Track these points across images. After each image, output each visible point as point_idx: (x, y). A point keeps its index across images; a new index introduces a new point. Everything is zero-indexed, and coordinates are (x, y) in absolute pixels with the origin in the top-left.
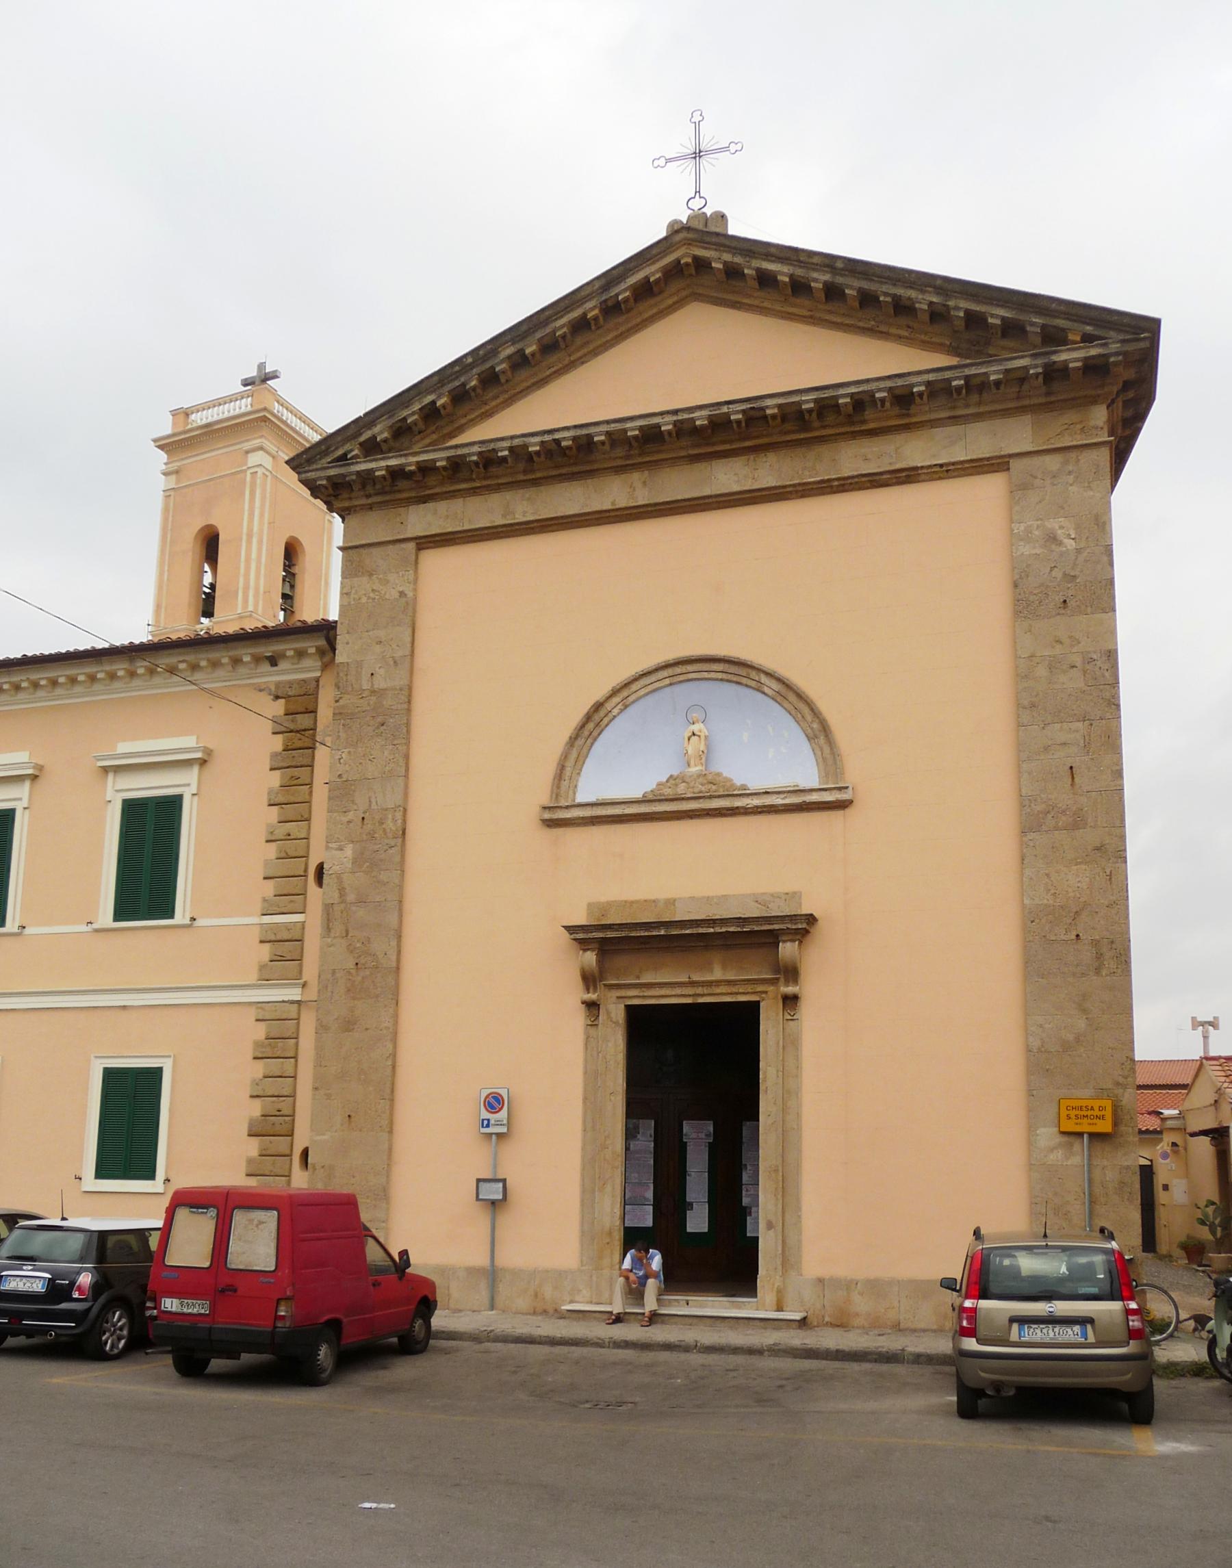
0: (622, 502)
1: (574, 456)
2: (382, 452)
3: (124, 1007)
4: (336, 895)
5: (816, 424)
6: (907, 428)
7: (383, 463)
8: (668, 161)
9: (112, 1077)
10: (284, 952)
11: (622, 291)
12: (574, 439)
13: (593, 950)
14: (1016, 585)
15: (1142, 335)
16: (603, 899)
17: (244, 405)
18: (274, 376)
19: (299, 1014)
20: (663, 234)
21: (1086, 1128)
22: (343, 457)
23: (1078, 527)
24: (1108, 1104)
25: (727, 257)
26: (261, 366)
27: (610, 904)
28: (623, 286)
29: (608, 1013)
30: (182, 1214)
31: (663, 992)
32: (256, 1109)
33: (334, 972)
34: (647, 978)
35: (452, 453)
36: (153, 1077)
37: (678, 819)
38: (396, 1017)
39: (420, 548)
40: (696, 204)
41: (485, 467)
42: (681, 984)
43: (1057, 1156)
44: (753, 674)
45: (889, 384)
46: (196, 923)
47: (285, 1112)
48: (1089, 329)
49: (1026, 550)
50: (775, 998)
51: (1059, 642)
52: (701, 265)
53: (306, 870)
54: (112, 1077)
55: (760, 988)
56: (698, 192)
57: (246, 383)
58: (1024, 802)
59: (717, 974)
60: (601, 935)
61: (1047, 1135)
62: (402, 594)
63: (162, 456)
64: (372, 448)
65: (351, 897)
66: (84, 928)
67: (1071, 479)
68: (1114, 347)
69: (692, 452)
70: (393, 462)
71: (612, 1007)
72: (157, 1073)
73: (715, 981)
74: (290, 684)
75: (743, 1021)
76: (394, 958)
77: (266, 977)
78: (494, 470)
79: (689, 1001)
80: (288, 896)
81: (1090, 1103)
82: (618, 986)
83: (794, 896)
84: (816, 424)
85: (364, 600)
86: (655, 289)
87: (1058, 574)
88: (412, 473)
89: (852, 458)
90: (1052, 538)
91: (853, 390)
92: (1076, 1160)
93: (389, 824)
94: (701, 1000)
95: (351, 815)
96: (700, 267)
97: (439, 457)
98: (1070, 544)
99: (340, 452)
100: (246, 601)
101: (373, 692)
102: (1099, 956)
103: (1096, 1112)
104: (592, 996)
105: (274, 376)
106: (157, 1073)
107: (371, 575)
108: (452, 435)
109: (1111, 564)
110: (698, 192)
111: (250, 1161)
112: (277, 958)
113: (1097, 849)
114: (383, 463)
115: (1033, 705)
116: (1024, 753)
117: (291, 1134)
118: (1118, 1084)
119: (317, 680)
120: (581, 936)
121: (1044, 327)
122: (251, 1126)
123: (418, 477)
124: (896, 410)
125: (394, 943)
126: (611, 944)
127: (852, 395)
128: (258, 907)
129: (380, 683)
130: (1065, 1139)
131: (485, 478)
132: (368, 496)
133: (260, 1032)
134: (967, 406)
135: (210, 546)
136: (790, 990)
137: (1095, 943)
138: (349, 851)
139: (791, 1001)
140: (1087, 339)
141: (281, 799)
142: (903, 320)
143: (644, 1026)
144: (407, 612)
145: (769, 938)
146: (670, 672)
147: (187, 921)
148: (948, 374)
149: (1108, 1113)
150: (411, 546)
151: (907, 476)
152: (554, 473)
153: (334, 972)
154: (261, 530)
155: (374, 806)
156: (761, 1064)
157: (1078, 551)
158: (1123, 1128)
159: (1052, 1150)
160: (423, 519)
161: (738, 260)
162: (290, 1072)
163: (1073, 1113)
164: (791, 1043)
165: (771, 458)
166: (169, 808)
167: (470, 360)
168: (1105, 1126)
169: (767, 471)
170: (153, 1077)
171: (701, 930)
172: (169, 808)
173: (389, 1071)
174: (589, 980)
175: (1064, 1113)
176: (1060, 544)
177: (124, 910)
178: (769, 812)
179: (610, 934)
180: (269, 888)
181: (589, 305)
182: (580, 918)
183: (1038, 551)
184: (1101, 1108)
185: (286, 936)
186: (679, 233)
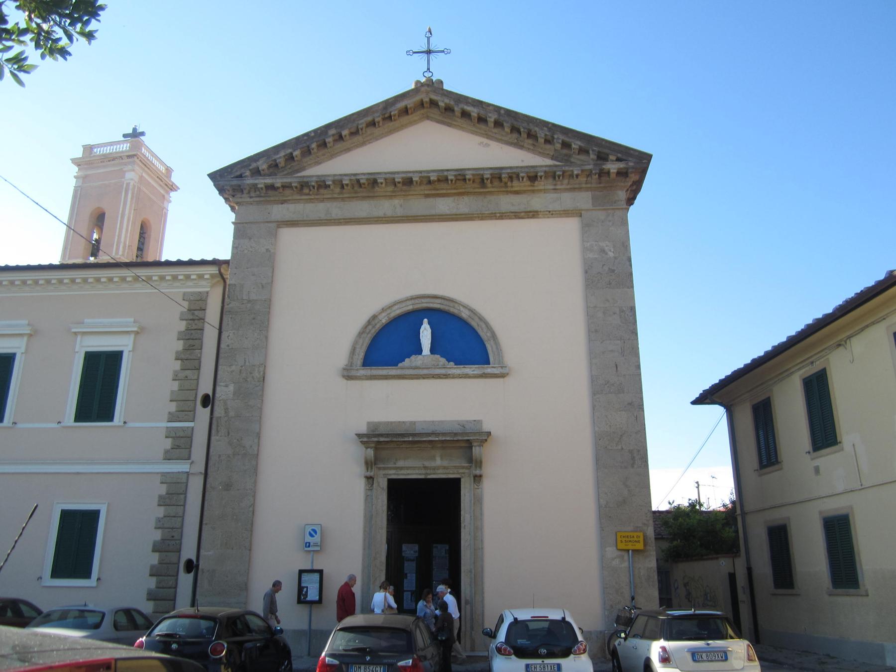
0: (389, 213)
1: (367, 186)
2: (261, 175)
3: (78, 473)
4: (223, 412)
5: (489, 185)
6: (533, 191)
7: (263, 181)
8: (443, 52)
9: (67, 516)
10: (180, 445)
11: (394, 111)
12: (367, 180)
13: (371, 448)
14: (586, 272)
15: (648, 157)
16: (376, 420)
17: (125, 147)
18: (143, 134)
19: (188, 480)
20: (413, 87)
21: (630, 547)
22: (241, 176)
23: (614, 247)
24: (641, 534)
25: (447, 101)
26: (135, 130)
27: (380, 423)
28: (393, 108)
29: (378, 483)
30: (317, 598)
31: (409, 472)
32: (158, 535)
33: (220, 456)
34: (401, 463)
35: (301, 180)
36: (92, 517)
37: (412, 379)
38: (255, 482)
39: (278, 227)
40: (428, 75)
41: (318, 189)
42: (419, 468)
43: (616, 562)
44: (456, 305)
45: (526, 170)
46: (127, 425)
47: (176, 537)
48: (619, 155)
49: (591, 255)
50: (469, 476)
51: (607, 300)
52: (433, 103)
53: (196, 397)
54: (67, 516)
55: (461, 471)
56: (429, 69)
57: (125, 136)
58: (593, 380)
59: (438, 462)
60: (376, 439)
61: (611, 551)
62: (267, 250)
63: (76, 169)
64: (257, 172)
65: (232, 414)
66: (55, 425)
67: (611, 224)
68: (631, 164)
69: (426, 192)
70: (285, 180)
71: (380, 480)
72: (95, 514)
73: (439, 467)
74: (192, 294)
75: (451, 488)
76: (256, 449)
77: (168, 456)
78: (322, 191)
79: (422, 477)
80: (184, 412)
81: (632, 534)
82: (384, 469)
83: (479, 422)
84: (489, 185)
85: (246, 252)
86: (410, 112)
87: (606, 268)
88: (278, 188)
89: (506, 202)
90: (603, 251)
91: (509, 171)
92: (626, 564)
93: (256, 374)
94: (429, 477)
95: (233, 368)
96: (431, 103)
97: (293, 180)
98: (611, 254)
99: (238, 173)
100: (118, 249)
101: (249, 301)
102: (633, 458)
103: (635, 539)
104: (369, 474)
105: (143, 134)
106: (95, 514)
107: (250, 239)
108: (298, 171)
109: (631, 265)
110: (429, 69)
111: (152, 567)
112: (176, 447)
113: (630, 404)
114: (263, 181)
115: (596, 331)
116: (592, 354)
117: (179, 551)
118: (644, 524)
119: (207, 293)
120: (365, 439)
121: (599, 152)
122: (154, 546)
123: (281, 190)
124: (529, 183)
125: (256, 441)
126: (381, 443)
127: (508, 173)
128: (166, 417)
129: (253, 297)
130: (620, 553)
131: (317, 195)
132: (251, 197)
133: (163, 490)
134: (562, 184)
135: (99, 219)
136: (478, 472)
137: (631, 452)
138: (231, 388)
139: (478, 478)
140: (619, 160)
141: (183, 356)
142: (530, 141)
143: (400, 492)
144: (269, 260)
145: (467, 443)
146: (413, 301)
147: (122, 424)
148: (555, 169)
149: (641, 539)
150: (273, 225)
151: (533, 214)
152: (433, 192)
153: (220, 456)
154: (130, 213)
155: (247, 364)
156: (462, 513)
157: (615, 258)
158: (648, 548)
159: (613, 559)
160: (279, 211)
161: (452, 103)
162: (181, 514)
163: (624, 539)
164: (478, 501)
165: (466, 199)
166: (113, 359)
167: (313, 134)
168: (640, 546)
169: (464, 204)
170: (92, 517)
171: (430, 439)
172: (113, 359)
173: (251, 514)
174: (369, 464)
175: (619, 539)
176: (607, 254)
177: (81, 416)
178: (465, 378)
179: (382, 439)
180: (173, 407)
181: (376, 115)
182: (363, 429)
183: (596, 256)
184: (638, 537)
185: (182, 434)
186: (419, 86)
